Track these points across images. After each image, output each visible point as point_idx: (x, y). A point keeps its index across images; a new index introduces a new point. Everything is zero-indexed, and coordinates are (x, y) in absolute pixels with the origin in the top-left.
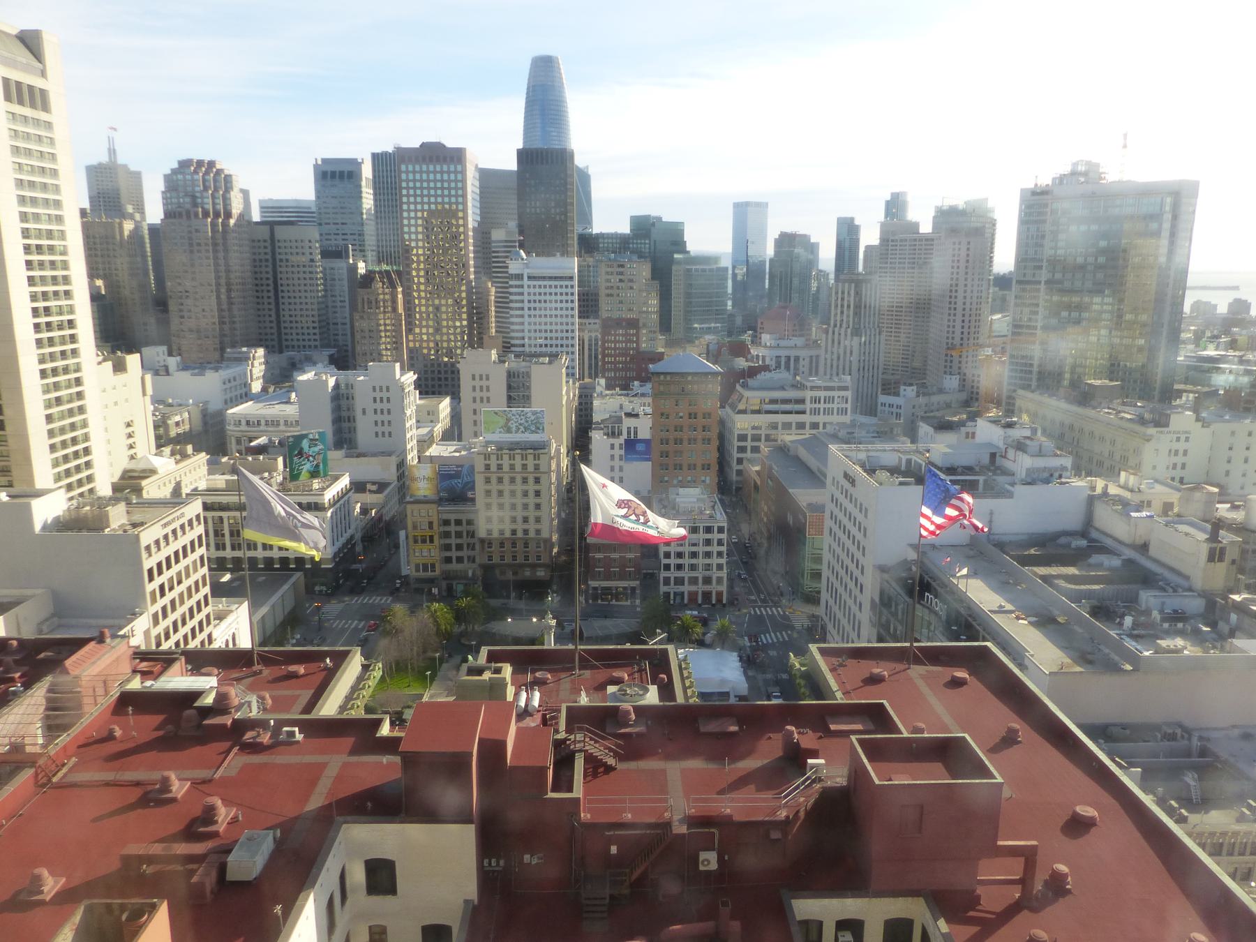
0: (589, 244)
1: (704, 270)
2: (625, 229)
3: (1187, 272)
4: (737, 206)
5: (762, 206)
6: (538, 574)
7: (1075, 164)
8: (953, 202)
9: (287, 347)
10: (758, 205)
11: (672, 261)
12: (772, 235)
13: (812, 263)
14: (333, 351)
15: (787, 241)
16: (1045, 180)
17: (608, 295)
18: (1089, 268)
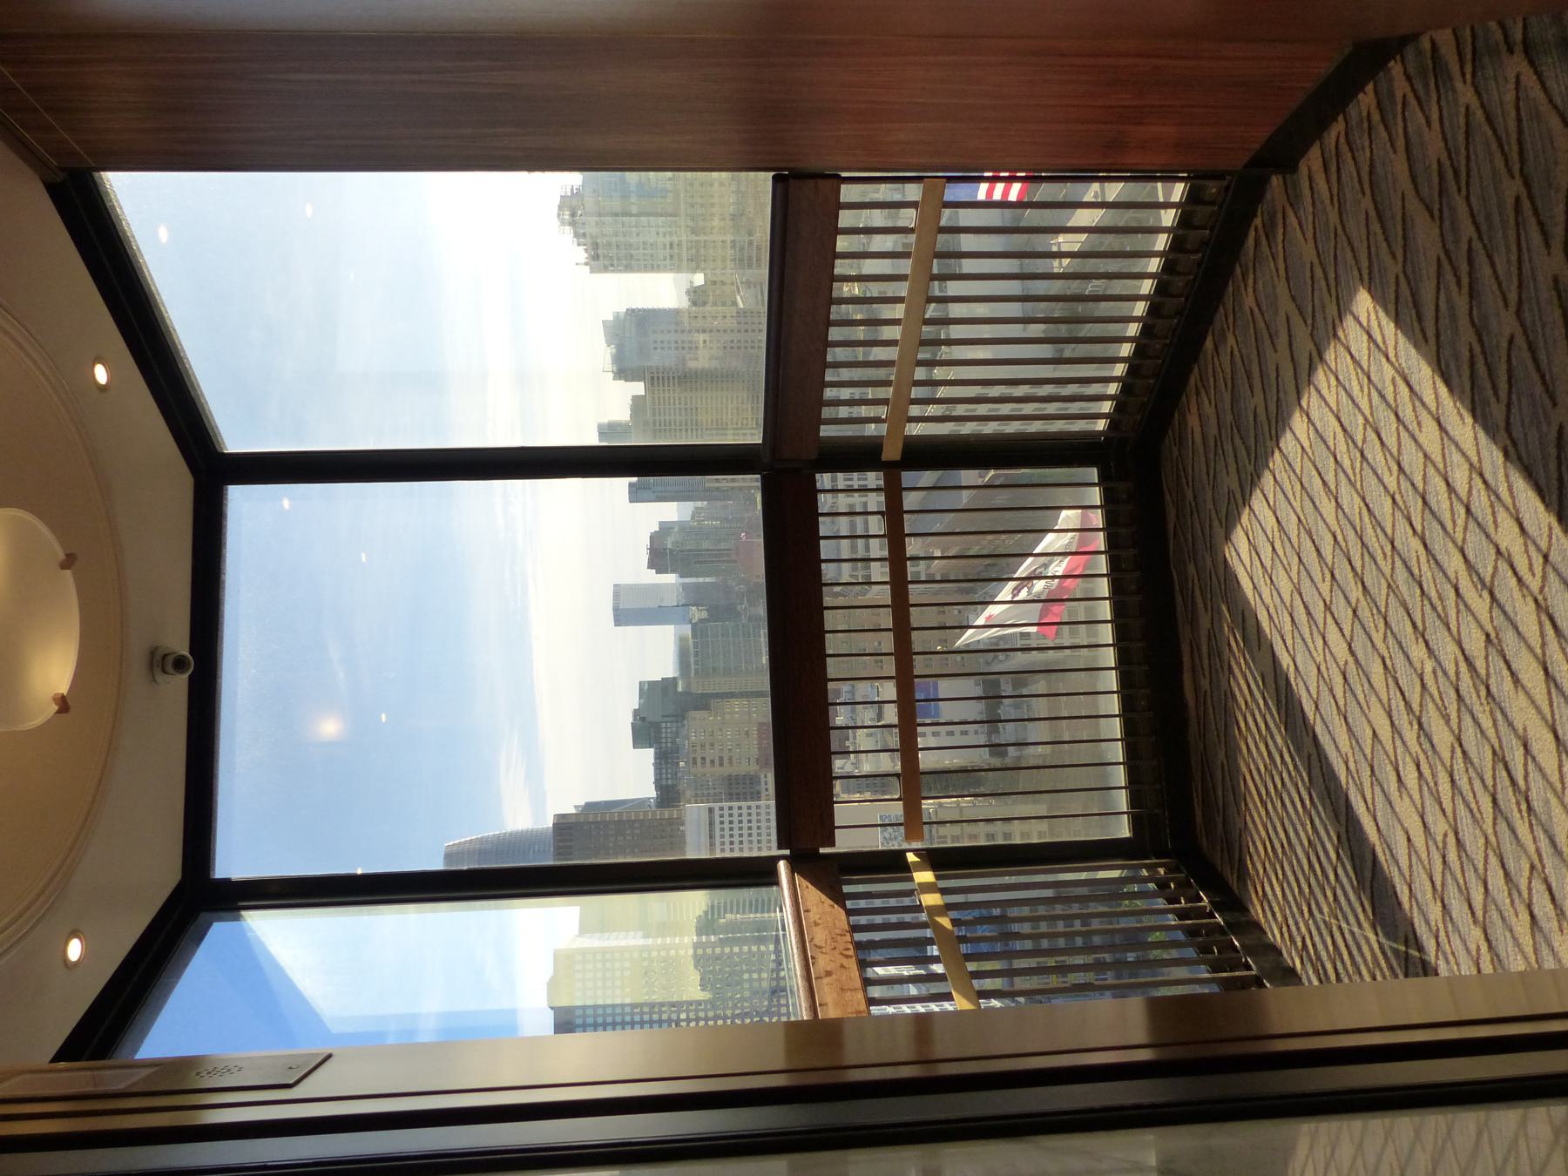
0: (668, 794)
1: (696, 654)
2: (649, 754)
5: (618, 591)
7: (563, 223)
8: (609, 359)
10: (616, 595)
11: (686, 693)
12: (652, 577)
13: (682, 525)
15: (660, 557)
16: (581, 254)
17: (731, 762)
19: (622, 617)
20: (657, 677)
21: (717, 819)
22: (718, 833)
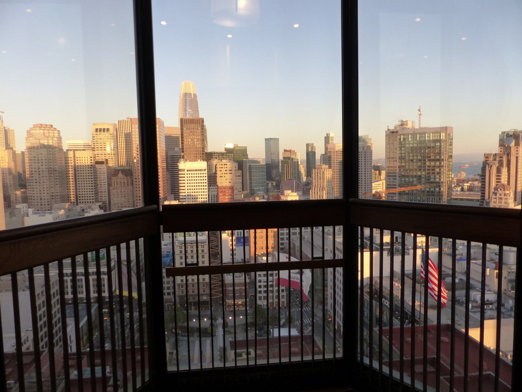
0: (208, 157)
3: (246, 150)
4: (266, 140)
5: (277, 140)
6: (204, 298)
9: (80, 202)
14: (100, 204)
18: (415, 161)
19: (268, 141)
20: (248, 152)
21: (202, 172)
22: (197, 172)
